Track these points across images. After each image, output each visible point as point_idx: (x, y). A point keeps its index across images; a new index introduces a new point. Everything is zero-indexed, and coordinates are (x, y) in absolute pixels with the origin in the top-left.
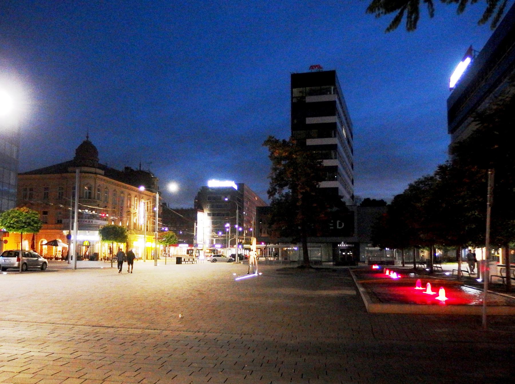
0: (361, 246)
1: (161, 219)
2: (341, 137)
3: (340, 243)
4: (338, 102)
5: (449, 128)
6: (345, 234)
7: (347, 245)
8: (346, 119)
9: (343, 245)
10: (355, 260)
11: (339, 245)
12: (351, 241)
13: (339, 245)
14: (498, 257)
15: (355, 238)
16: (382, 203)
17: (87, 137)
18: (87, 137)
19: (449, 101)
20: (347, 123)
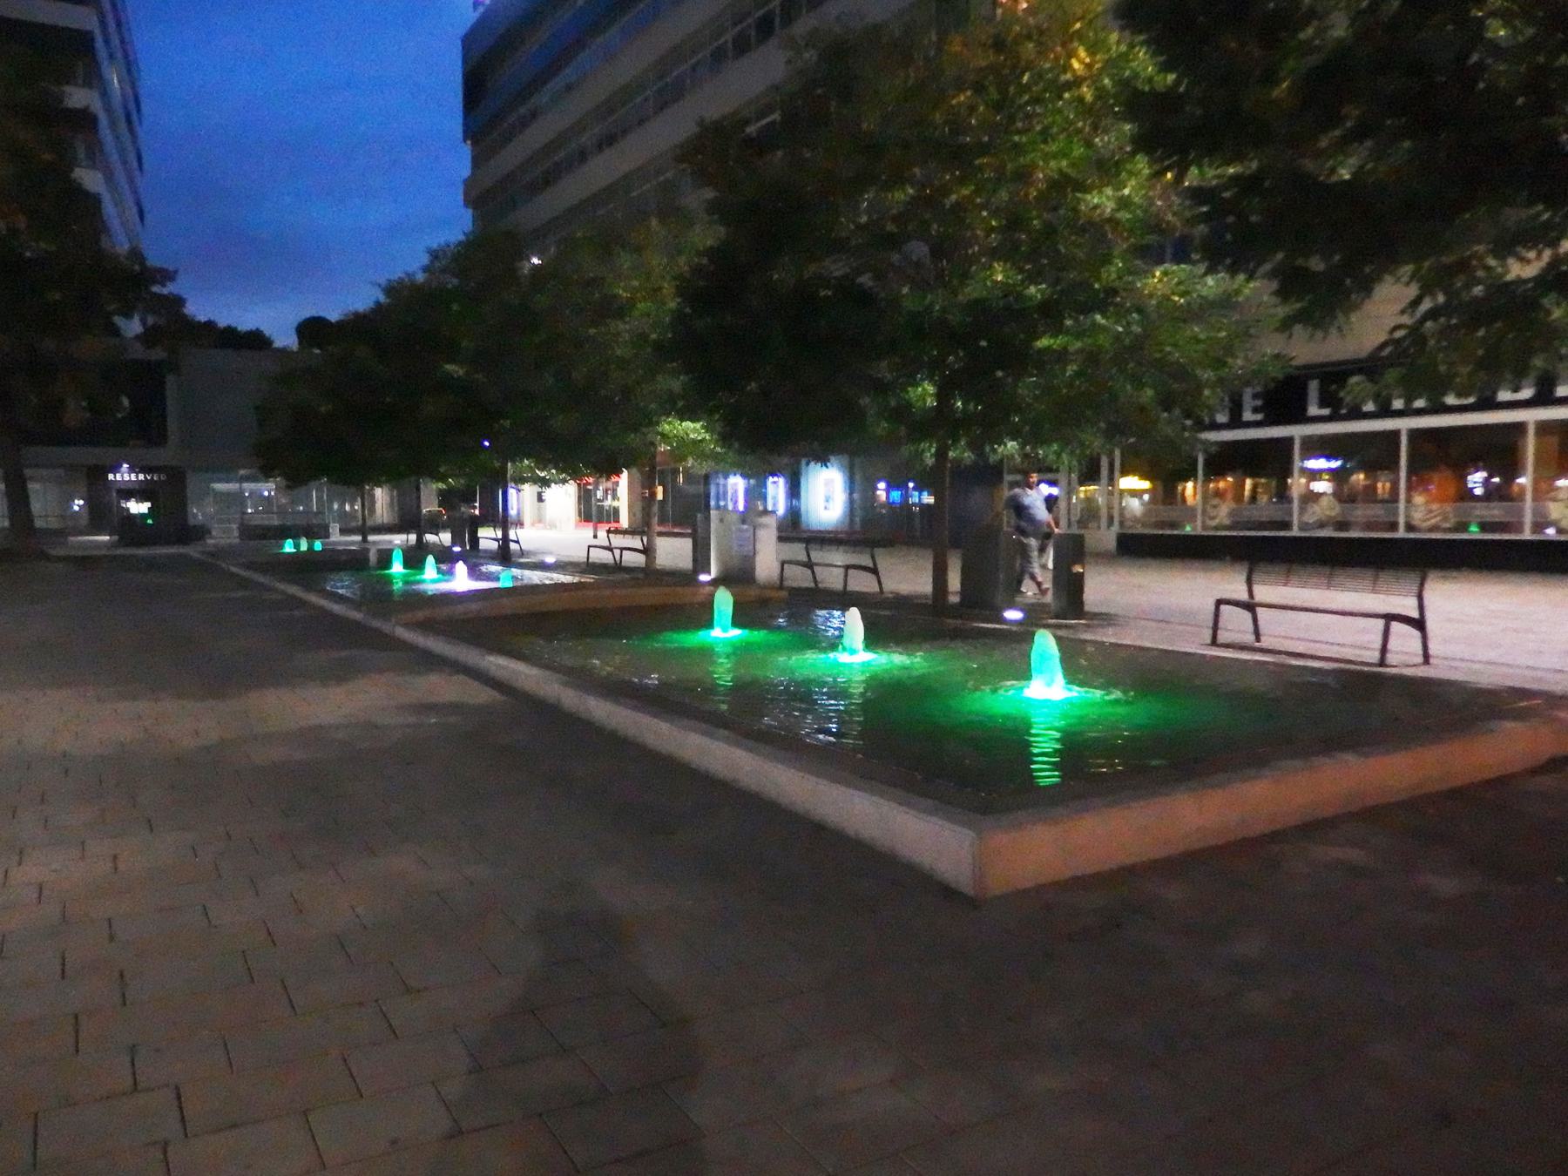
0: (193, 483)
1: (1259, 403)
2: (105, 94)
3: (115, 469)
4: (97, 32)
5: (466, 125)
6: (143, 429)
7: (141, 477)
8: (122, 42)
9: (124, 475)
10: (173, 523)
11: (111, 476)
12: (155, 463)
13: (111, 476)
14: (616, 511)
15: (166, 455)
16: (256, 341)
17: (540, 499)
18: (540, 499)
19: (468, 41)
20: (126, 56)
